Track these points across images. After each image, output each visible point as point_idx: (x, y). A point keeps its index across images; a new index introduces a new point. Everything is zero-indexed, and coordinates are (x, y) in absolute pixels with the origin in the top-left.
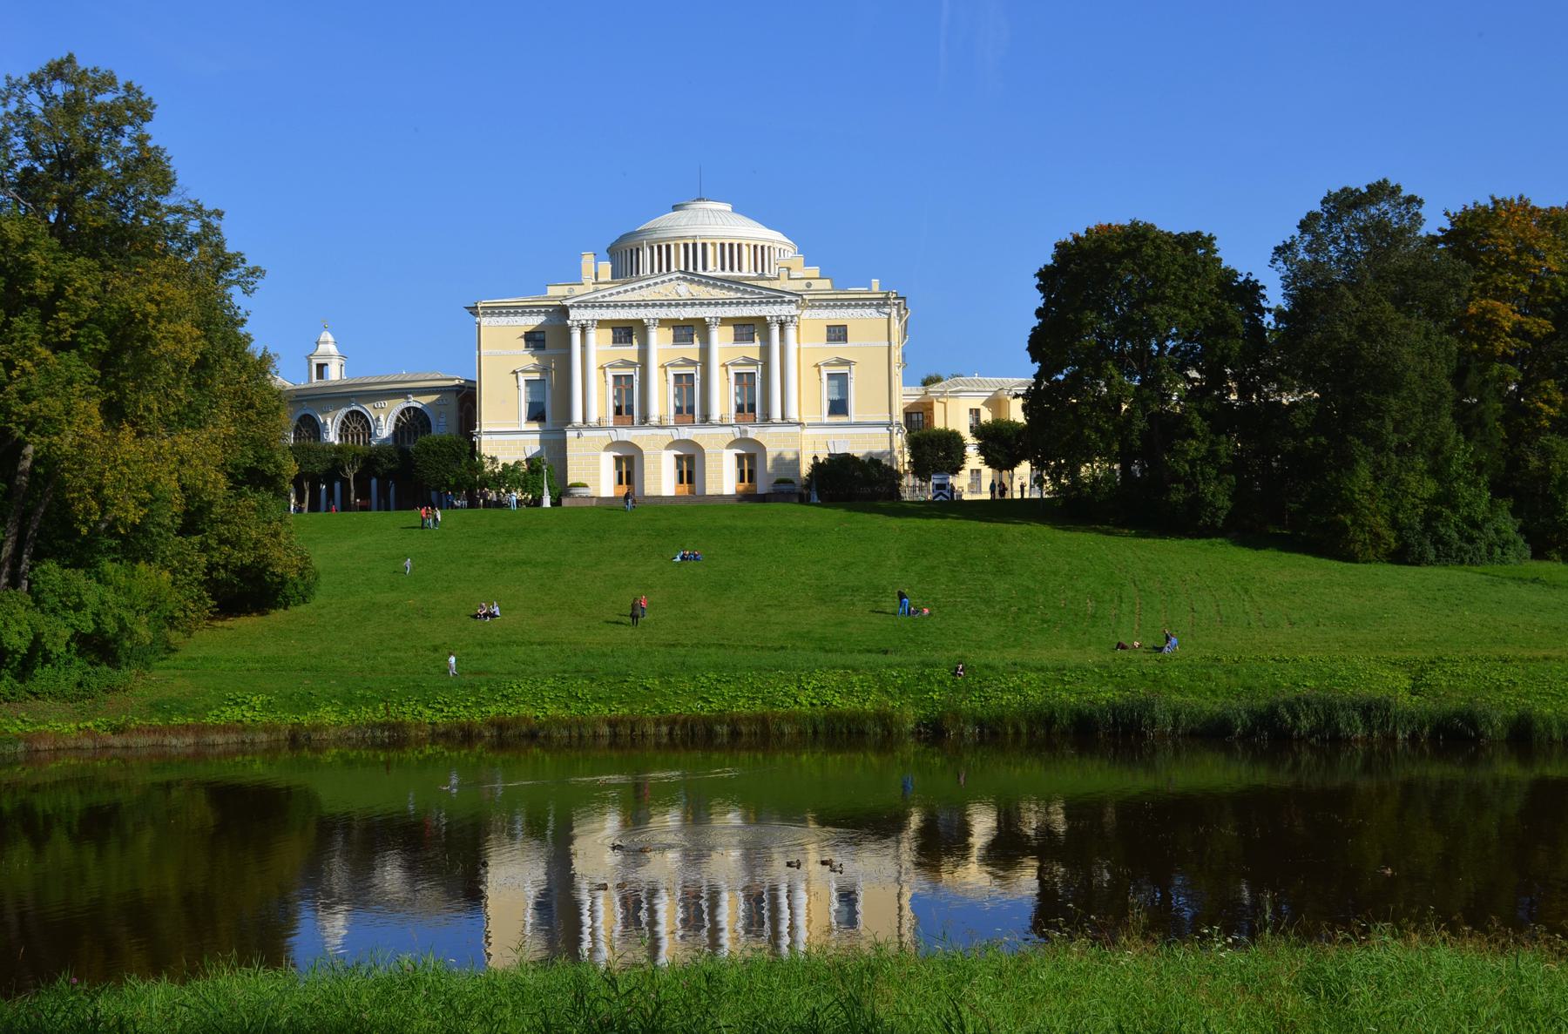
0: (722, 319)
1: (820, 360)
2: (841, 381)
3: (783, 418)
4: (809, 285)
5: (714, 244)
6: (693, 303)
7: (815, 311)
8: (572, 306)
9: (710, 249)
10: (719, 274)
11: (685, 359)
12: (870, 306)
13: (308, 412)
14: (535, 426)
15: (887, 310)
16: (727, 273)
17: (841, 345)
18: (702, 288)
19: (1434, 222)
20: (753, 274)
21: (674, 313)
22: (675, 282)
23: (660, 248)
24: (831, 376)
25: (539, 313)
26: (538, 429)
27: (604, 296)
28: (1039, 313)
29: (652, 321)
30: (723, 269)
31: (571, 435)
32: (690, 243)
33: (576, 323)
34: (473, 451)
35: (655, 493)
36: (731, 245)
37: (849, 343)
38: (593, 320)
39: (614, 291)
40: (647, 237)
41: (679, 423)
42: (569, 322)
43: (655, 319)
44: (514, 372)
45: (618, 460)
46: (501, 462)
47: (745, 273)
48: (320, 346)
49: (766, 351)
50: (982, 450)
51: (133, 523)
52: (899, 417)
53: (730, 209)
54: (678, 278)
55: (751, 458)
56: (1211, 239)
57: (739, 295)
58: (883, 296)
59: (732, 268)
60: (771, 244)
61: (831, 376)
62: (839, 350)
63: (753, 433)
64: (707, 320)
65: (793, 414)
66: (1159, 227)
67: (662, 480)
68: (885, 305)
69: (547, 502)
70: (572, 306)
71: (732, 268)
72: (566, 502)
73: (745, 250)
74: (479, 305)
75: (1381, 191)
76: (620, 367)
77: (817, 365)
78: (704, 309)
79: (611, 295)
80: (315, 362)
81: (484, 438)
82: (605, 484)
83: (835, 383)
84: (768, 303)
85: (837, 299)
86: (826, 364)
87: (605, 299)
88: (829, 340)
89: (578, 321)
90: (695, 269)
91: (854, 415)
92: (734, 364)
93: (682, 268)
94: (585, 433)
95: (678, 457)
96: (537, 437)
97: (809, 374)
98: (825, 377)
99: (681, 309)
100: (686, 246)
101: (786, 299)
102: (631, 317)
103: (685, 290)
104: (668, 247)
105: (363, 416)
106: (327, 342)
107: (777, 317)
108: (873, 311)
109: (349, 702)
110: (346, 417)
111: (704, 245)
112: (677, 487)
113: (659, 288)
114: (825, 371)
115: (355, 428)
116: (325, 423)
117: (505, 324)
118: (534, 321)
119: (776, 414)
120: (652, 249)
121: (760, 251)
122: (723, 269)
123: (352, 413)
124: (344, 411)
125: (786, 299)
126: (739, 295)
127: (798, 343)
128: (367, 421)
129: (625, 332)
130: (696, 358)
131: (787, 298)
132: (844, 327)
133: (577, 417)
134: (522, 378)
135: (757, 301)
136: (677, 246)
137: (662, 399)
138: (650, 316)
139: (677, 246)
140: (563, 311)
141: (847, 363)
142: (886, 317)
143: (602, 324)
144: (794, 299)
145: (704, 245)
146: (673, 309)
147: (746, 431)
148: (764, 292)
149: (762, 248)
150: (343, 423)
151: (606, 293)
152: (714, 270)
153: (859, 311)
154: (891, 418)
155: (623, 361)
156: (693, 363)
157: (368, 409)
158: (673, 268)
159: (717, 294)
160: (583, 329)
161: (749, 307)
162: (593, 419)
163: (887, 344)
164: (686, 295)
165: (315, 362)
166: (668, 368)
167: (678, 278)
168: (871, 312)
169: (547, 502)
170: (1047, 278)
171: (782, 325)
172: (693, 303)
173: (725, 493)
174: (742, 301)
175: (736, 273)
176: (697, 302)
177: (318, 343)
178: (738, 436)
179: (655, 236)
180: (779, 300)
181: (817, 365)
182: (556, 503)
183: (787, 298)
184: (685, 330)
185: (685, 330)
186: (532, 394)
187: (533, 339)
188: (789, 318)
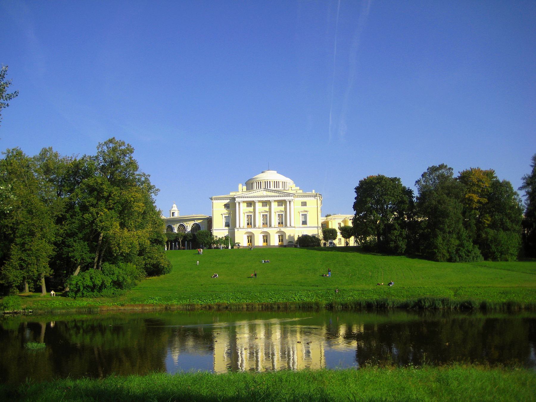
0: (243, 201)
2: (305, 216)
4: (296, 192)
5: (272, 181)
8: (236, 198)
9: (280, 183)
11: (265, 211)
12: (312, 197)
14: (227, 228)
16: (276, 189)
18: (269, 192)
19: (456, 174)
20: (283, 189)
24: (302, 215)
25: (228, 199)
27: (244, 195)
28: (356, 198)
30: (275, 188)
31: (236, 230)
32: (266, 181)
33: (237, 202)
36: (277, 182)
38: (242, 201)
41: (263, 227)
46: (218, 237)
47: (280, 189)
49: (286, 208)
50: (341, 233)
52: (320, 225)
54: (263, 190)
55: (251, 237)
56: (399, 179)
57: (279, 194)
58: (316, 194)
59: (277, 188)
62: (304, 208)
63: (283, 229)
65: (293, 225)
67: (259, 242)
68: (316, 196)
69: (230, 247)
70: (236, 198)
71: (277, 188)
75: (442, 167)
76: (304, 212)
77: (222, 214)
79: (246, 194)
81: (214, 231)
84: (286, 196)
91: (308, 225)
94: (240, 230)
96: (228, 231)
98: (301, 215)
103: (265, 193)
104: (261, 182)
108: (313, 198)
118: (227, 201)
119: (288, 225)
121: (284, 183)
122: (275, 188)
126: (279, 194)
130: (268, 210)
131: (291, 195)
138: (256, 200)
141: (307, 211)
143: (244, 202)
144: (293, 195)
145: (270, 182)
151: (245, 194)
152: (272, 188)
154: (318, 225)
156: (267, 212)
158: (262, 188)
159: (273, 194)
160: (239, 203)
162: (241, 226)
164: (265, 194)
167: (263, 190)
169: (230, 247)
170: (358, 189)
171: (290, 202)
174: (280, 196)
175: (278, 189)
176: (268, 196)
179: (257, 179)
180: (289, 195)
182: (232, 248)
184: (265, 203)
187: (227, 206)
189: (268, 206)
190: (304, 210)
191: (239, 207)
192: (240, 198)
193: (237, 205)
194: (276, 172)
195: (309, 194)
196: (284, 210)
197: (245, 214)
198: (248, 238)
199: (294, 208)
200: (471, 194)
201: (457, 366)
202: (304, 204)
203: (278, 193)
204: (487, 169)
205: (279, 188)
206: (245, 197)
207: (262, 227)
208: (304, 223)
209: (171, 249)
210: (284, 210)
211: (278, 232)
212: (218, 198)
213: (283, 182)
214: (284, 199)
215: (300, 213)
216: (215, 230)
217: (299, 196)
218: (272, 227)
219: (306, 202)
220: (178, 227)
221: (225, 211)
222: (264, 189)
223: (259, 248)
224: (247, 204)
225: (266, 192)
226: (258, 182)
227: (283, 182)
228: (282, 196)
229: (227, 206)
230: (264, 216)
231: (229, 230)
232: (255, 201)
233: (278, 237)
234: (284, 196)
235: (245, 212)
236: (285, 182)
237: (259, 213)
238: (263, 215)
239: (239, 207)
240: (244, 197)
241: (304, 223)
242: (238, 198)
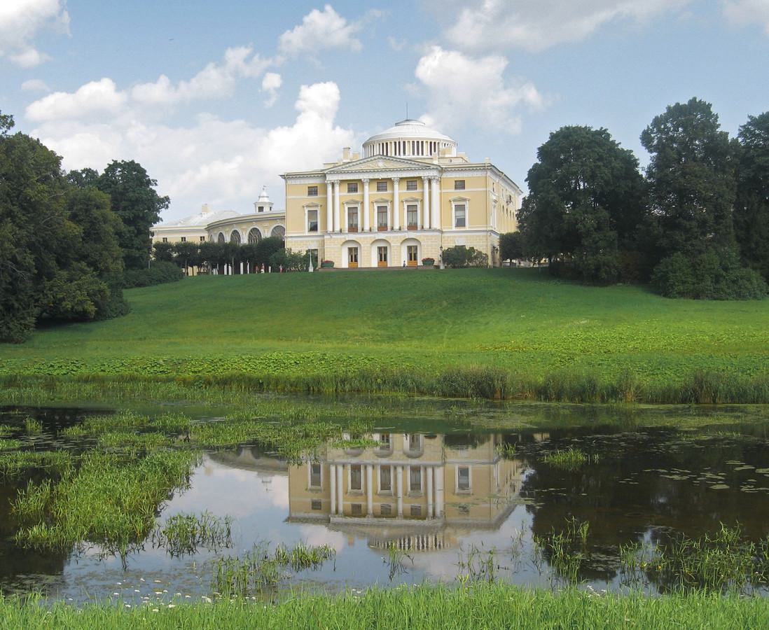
2: (460, 208)
5: (427, 142)
6: (386, 170)
10: (411, 156)
16: (416, 156)
21: (377, 176)
30: (414, 154)
35: (367, 266)
36: (418, 142)
37: (466, 190)
47: (425, 156)
49: (423, 193)
51: (463, 421)
55: (356, 249)
59: (418, 154)
62: (461, 193)
66: (157, 193)
67: (369, 260)
71: (418, 154)
76: (381, 202)
82: (374, 263)
88: (456, 188)
90: (396, 154)
91: (467, 228)
93: (385, 154)
94: (334, 237)
98: (307, 212)
100: (395, 143)
103: (381, 164)
109: (305, 512)
111: (422, 142)
112: (349, 264)
119: (427, 226)
122: (414, 154)
123: (254, 229)
129: (353, 186)
130: (419, 197)
131: (432, 167)
132: (463, 182)
133: (330, 229)
136: (391, 143)
137: (399, 217)
141: (464, 200)
145: (404, 142)
148: (420, 164)
149: (435, 143)
152: (409, 155)
160: (333, 185)
171: (430, 181)
172: (386, 170)
173: (373, 266)
183: (432, 167)
184: (382, 184)
185: (382, 184)
193: (330, 188)
200: (529, 401)
201: (726, 248)
204: (509, 462)
208: (461, 222)
209: (254, 272)
213: (431, 143)
214: (418, 175)
220: (250, 234)
223: (370, 271)
226: (383, 144)
227: (431, 143)
235: (403, 199)
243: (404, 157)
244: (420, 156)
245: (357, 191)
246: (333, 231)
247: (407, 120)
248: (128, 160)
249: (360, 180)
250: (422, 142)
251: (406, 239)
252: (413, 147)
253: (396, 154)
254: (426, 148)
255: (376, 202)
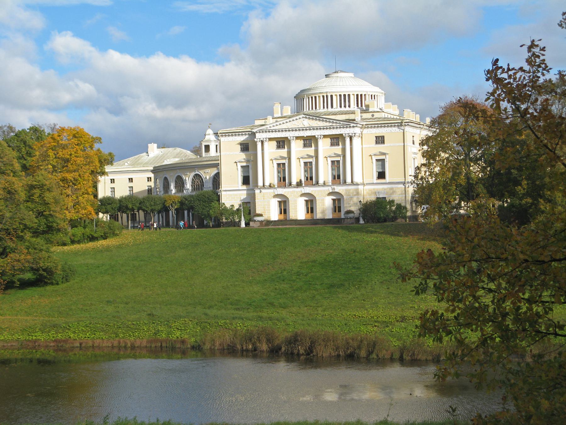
0: (323, 135)
1: (372, 153)
3: (352, 182)
4: (373, 116)
5: (336, 95)
7: (370, 130)
8: (257, 132)
9: (334, 98)
11: (308, 155)
12: (395, 126)
13: (179, 174)
14: (245, 187)
15: (403, 128)
16: (343, 109)
17: (382, 145)
18: (314, 121)
21: (301, 134)
22: (302, 119)
23: (312, 98)
24: (377, 160)
25: (246, 134)
26: (245, 188)
27: (270, 127)
29: (292, 138)
30: (341, 107)
31: (257, 191)
32: (325, 95)
33: (258, 140)
34: (218, 198)
36: (345, 95)
37: (386, 145)
38: (266, 138)
39: (284, 122)
40: (307, 93)
41: (279, 186)
42: (255, 140)
43: (293, 137)
44: (235, 162)
45: (280, 202)
48: (206, 136)
49: (344, 150)
53: (353, 76)
54: (303, 117)
55: (339, 200)
57: (331, 124)
58: (400, 121)
59: (345, 107)
60: (366, 93)
61: (377, 160)
62: (381, 148)
64: (316, 136)
68: (401, 125)
69: (243, 225)
70: (257, 132)
71: (345, 107)
72: (252, 224)
73: (352, 97)
74: (219, 132)
77: (370, 156)
78: (315, 131)
79: (274, 126)
80: (204, 144)
81: (223, 193)
82: (274, 215)
83: (380, 163)
84: (343, 127)
85: (378, 124)
86: (375, 155)
87: (271, 128)
89: (260, 139)
91: (388, 179)
92: (330, 157)
94: (263, 191)
95: (306, 201)
96: (245, 192)
97: (367, 159)
99: (304, 131)
100: (323, 96)
101: (352, 126)
102: (283, 136)
103: (307, 123)
104: (315, 97)
105: (200, 177)
106: (209, 134)
107: (348, 134)
108: (396, 128)
110: (194, 177)
111: (332, 96)
112: (306, 215)
113: (295, 122)
114: (374, 158)
115: (197, 182)
116: (186, 179)
117: (231, 140)
118: (242, 138)
119: (349, 180)
120: (309, 98)
122: (341, 107)
123: (196, 175)
124: (193, 174)
125: (352, 126)
126: (331, 124)
127: (362, 145)
128: (202, 179)
129: (282, 143)
133: (260, 183)
134: (239, 165)
135: (338, 127)
136: (319, 97)
138: (291, 135)
139: (319, 97)
140: (253, 134)
141: (384, 154)
142: (402, 131)
143: (271, 139)
145: (332, 96)
146: (301, 132)
147: (334, 189)
148: (342, 123)
150: (193, 180)
151: (271, 126)
153: (390, 129)
154: (405, 180)
155: (281, 157)
156: (312, 157)
157: (201, 173)
159: (321, 124)
160: (262, 142)
161: (335, 130)
162: (267, 184)
163: (403, 144)
165: (204, 144)
166: (301, 159)
167: (303, 117)
168: (395, 129)
169: (243, 225)
171: (351, 138)
173: (299, 219)
174: (332, 127)
176: (311, 128)
177: (205, 135)
178: (331, 191)
179: (310, 92)
180: (348, 126)
181: (370, 156)
182: (247, 224)
184: (309, 141)
185: (309, 141)
186: (243, 172)
188: (354, 135)
189: (313, 145)
190: (380, 152)
191: (263, 150)
192: (263, 132)
193: (259, 145)
194: (352, 75)
195: (391, 122)
196: (313, 155)
197: (273, 162)
198: (280, 206)
199: (362, 148)
202: (380, 140)
203: (330, 122)
205: (332, 107)
206: (272, 131)
207: (330, 184)
208: (381, 175)
210: (313, 155)
211: (330, 194)
212: (232, 132)
215: (373, 156)
216: (226, 191)
217: (370, 126)
218: (319, 186)
219: (383, 137)
221: (242, 156)
222: (304, 116)
224: (331, 140)
225: (307, 120)
227: (357, 95)
228: (337, 128)
229: (245, 147)
230: (307, 166)
231: (248, 190)
232: (289, 138)
233: (277, 204)
234: (340, 127)
236: (374, 96)
237: (325, 157)
238: (279, 165)
239: (263, 150)
240: (269, 132)
241: (381, 175)
242: (260, 132)
243: (333, 110)
244: (347, 108)
245: (248, 150)
246: (264, 185)
247: (335, 72)
248: (73, 126)
249: (342, 135)
250: (349, 95)
251: (305, 194)
252: (341, 100)
253: (309, 109)
254: (353, 100)
255: (375, 155)
